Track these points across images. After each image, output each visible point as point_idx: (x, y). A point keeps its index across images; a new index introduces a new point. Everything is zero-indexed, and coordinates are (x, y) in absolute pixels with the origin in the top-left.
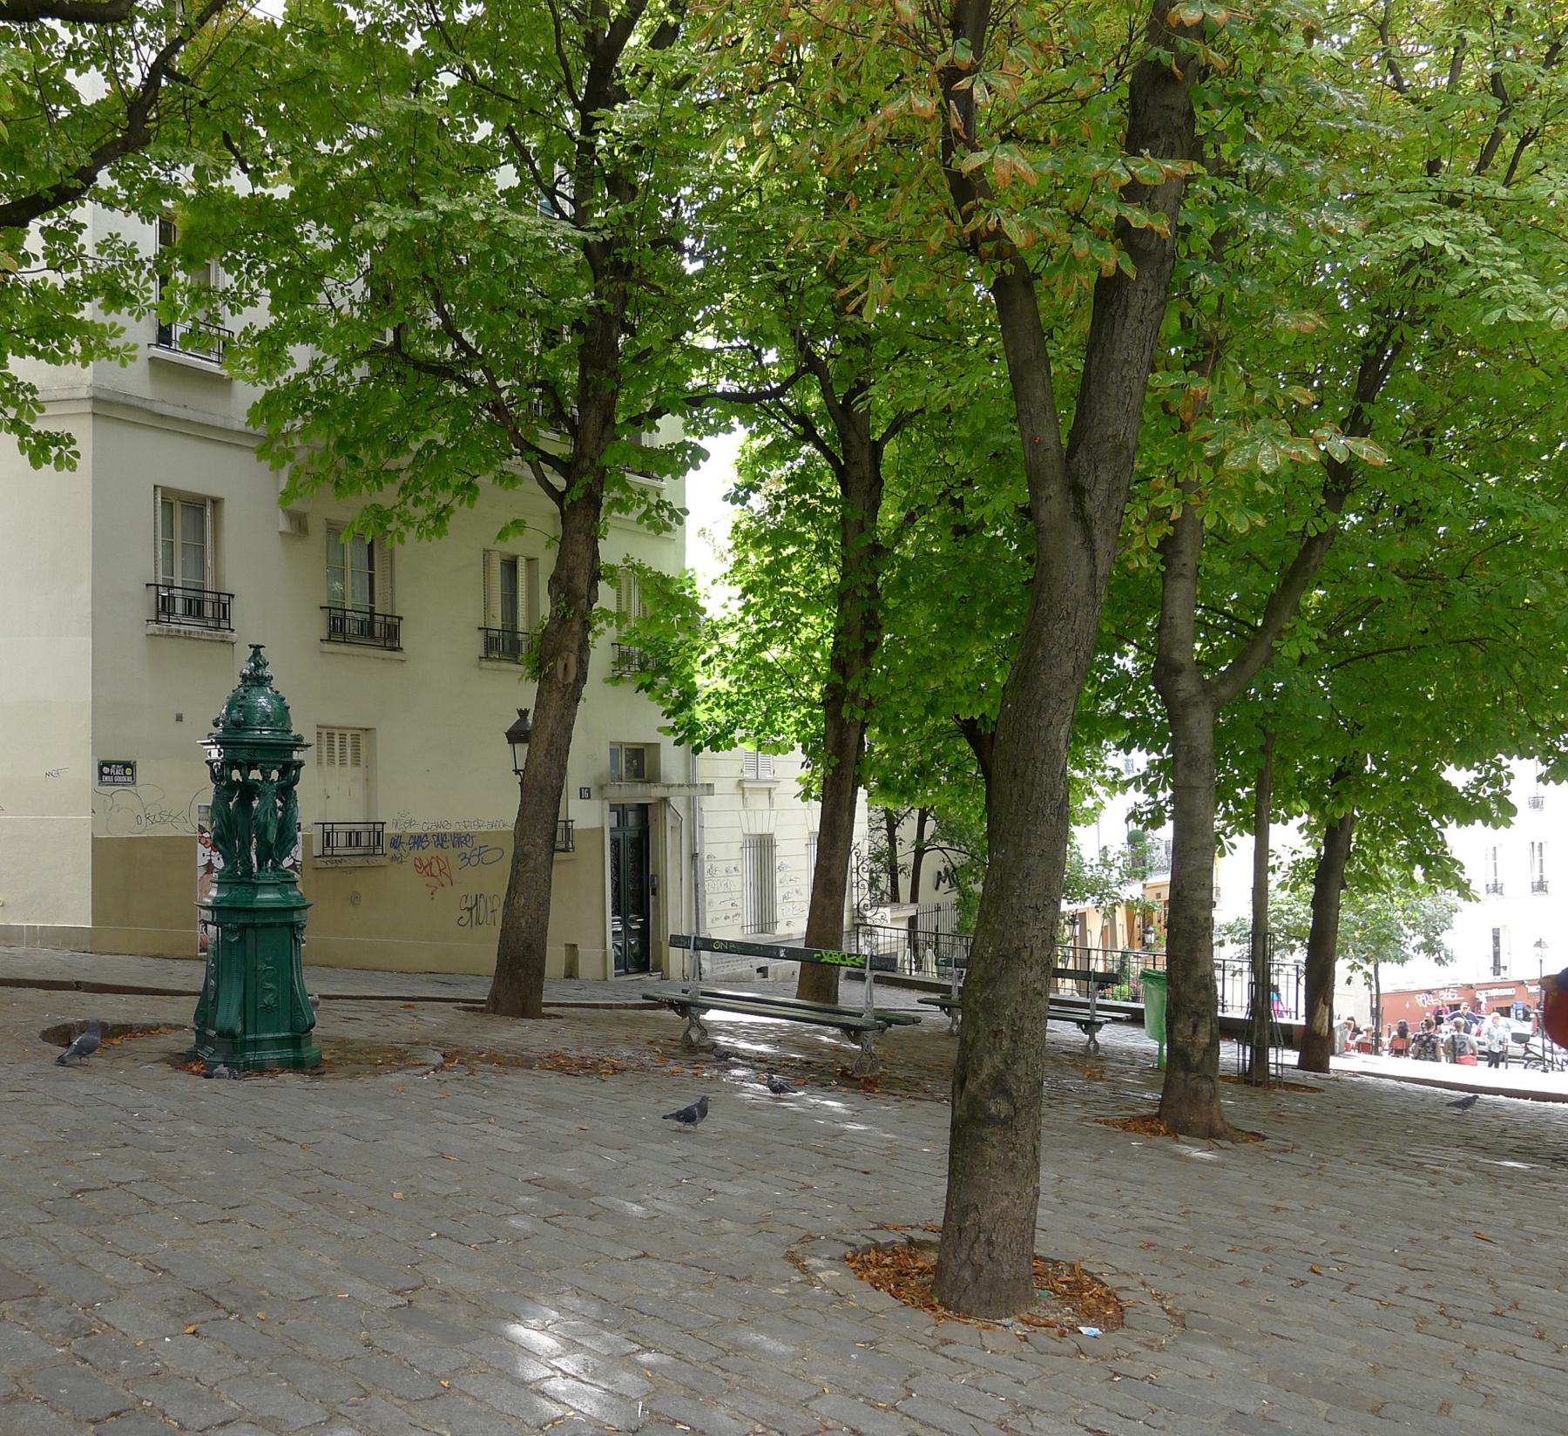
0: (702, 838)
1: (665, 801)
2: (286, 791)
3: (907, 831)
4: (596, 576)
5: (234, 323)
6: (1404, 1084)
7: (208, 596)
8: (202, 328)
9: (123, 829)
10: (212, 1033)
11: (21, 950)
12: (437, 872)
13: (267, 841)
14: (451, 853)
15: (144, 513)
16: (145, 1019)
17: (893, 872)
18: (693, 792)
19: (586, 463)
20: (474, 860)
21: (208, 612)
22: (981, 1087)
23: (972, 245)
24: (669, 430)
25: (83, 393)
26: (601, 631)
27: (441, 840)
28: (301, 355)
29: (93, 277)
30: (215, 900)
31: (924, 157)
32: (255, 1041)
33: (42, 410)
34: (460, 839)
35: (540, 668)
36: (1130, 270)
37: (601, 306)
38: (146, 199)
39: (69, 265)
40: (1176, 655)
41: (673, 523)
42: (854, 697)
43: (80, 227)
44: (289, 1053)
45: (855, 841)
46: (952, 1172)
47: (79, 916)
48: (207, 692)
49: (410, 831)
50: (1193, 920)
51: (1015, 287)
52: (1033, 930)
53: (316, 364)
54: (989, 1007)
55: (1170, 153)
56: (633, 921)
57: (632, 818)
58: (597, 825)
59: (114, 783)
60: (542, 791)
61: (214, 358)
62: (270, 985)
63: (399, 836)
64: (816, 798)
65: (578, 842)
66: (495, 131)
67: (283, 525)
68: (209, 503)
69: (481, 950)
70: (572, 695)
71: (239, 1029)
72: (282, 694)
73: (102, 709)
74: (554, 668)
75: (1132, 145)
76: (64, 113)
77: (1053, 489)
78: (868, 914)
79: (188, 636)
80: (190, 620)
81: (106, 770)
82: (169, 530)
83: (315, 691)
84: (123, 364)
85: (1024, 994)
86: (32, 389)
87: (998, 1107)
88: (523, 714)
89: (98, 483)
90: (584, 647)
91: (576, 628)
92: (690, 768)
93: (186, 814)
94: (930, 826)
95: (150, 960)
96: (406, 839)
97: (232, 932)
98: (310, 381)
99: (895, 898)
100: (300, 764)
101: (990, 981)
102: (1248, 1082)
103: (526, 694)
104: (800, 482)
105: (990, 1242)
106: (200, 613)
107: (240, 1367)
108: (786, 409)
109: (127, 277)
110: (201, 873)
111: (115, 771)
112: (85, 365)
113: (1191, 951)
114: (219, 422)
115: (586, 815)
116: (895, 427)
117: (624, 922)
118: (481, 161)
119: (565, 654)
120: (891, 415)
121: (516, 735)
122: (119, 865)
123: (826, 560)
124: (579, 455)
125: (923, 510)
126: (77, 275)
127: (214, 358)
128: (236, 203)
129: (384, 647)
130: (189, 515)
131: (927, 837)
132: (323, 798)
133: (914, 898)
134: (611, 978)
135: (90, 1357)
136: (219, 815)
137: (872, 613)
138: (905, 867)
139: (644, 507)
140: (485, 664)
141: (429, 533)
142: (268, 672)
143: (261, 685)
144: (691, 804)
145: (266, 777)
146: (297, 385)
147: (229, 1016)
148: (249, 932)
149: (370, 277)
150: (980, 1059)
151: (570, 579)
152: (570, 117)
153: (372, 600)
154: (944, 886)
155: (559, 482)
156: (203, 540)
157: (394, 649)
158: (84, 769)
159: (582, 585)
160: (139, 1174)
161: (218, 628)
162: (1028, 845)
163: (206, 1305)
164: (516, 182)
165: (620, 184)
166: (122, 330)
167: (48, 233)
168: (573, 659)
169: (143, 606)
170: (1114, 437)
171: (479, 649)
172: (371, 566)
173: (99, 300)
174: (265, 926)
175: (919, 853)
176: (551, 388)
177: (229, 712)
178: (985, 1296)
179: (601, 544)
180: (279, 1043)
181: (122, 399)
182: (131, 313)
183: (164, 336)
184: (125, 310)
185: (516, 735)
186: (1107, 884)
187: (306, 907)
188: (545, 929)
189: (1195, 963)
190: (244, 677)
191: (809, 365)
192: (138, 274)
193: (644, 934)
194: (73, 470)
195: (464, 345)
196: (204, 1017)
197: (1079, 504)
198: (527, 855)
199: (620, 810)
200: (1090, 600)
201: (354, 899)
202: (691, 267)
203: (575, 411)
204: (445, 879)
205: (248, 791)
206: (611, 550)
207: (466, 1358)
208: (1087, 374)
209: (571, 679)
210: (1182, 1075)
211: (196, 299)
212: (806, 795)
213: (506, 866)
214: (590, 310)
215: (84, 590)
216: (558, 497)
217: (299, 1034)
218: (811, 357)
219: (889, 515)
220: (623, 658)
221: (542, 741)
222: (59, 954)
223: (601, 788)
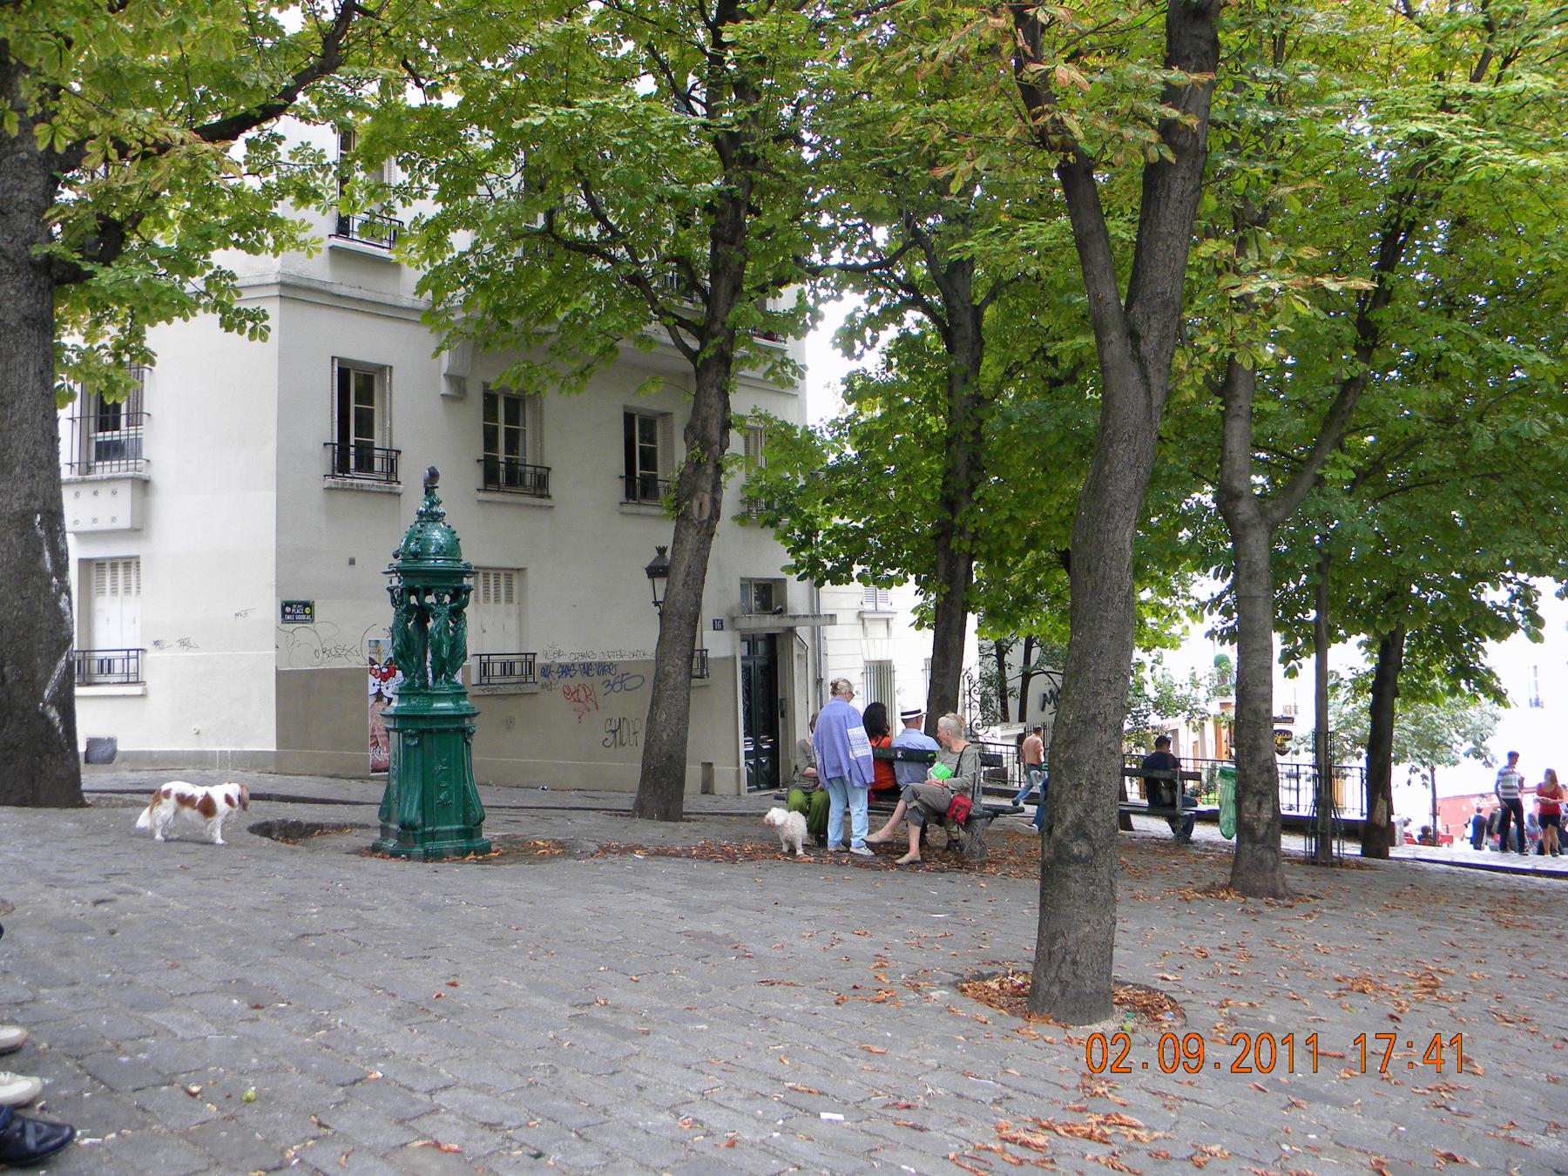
1: (791, 631)
2: (457, 613)
3: (1015, 657)
4: (726, 426)
5: (405, 214)
6: (1455, 869)
8: (378, 220)
9: (304, 662)
12: (583, 698)
14: (596, 681)
16: (333, 820)
17: (1003, 696)
18: (818, 621)
19: (717, 326)
20: (617, 687)
22: (1066, 833)
23: (1041, 140)
24: (785, 300)
25: (272, 280)
26: (733, 473)
27: (587, 669)
28: (461, 240)
29: (288, 179)
30: (397, 709)
31: (1004, 70)
32: (432, 833)
33: (239, 295)
34: (604, 668)
35: (677, 507)
36: (1170, 156)
37: (730, 191)
38: (335, 111)
39: (266, 169)
40: (1236, 484)
41: (796, 378)
42: (962, 531)
43: (281, 139)
44: (462, 843)
45: (965, 665)
46: (1042, 906)
48: (376, 539)
49: (558, 661)
50: (1256, 712)
51: (1076, 174)
52: (1106, 699)
53: (476, 245)
54: (1070, 764)
55: (1199, 70)
56: (763, 741)
57: (761, 646)
58: (728, 653)
59: (295, 621)
60: (680, 621)
61: (386, 244)
63: (549, 666)
64: (929, 627)
65: (712, 669)
66: (637, 48)
67: (444, 388)
69: (627, 768)
70: (707, 531)
72: (454, 528)
73: (287, 557)
74: (688, 507)
75: (1168, 65)
76: (268, 43)
77: (1114, 335)
78: (980, 732)
79: (360, 490)
80: (363, 475)
81: (288, 609)
83: (479, 531)
84: (310, 255)
85: (1100, 753)
86: (232, 276)
87: (1079, 848)
88: (662, 551)
89: (284, 356)
90: (717, 487)
91: (710, 470)
92: (815, 601)
94: (1036, 652)
95: (327, 780)
96: (554, 668)
97: (412, 736)
98: (471, 258)
99: (1005, 719)
100: (468, 591)
101: (1070, 743)
102: (1314, 864)
103: (665, 533)
104: (907, 343)
105: (1074, 962)
107: (452, 1053)
108: (898, 280)
109: (316, 178)
110: (371, 700)
111: (295, 611)
112: (276, 255)
113: (1255, 739)
114: (389, 300)
115: (719, 645)
116: (992, 296)
117: (756, 743)
118: (623, 74)
120: (990, 283)
121: (655, 572)
122: (299, 694)
123: (934, 411)
124: (712, 316)
125: (1020, 366)
126: (272, 178)
127: (386, 244)
128: (412, 112)
129: (534, 495)
130: (357, 388)
131: (1033, 662)
132: (487, 630)
133: (1022, 718)
134: (744, 793)
135: (332, 1044)
137: (977, 457)
138: (1014, 689)
139: (769, 364)
142: (440, 509)
143: (435, 521)
144: (816, 635)
145: (440, 601)
146: (460, 262)
147: (413, 814)
148: (426, 737)
149: (527, 170)
150: (1065, 809)
151: (704, 428)
152: (701, 35)
154: (1050, 708)
155: (694, 344)
157: (542, 496)
158: (271, 611)
159: (714, 432)
160: (353, 924)
162: (1101, 628)
163: (414, 1012)
164: (654, 89)
165: (743, 89)
166: (310, 225)
167: (250, 144)
168: (707, 499)
169: (322, 461)
170: (1163, 293)
173: (290, 199)
174: (440, 731)
175: (1026, 677)
176: (684, 262)
177: (407, 544)
178: (1071, 1007)
179: (732, 397)
181: (305, 283)
182: (318, 209)
183: (343, 228)
184: (313, 206)
185: (655, 572)
186: (1196, 701)
187: (475, 715)
188: (684, 742)
189: (1258, 749)
190: (420, 514)
191: (914, 240)
192: (326, 175)
193: (774, 753)
194: (265, 340)
195: (609, 227)
196: (386, 811)
197: (1136, 347)
198: (668, 675)
199: (750, 640)
200: (1148, 427)
201: (509, 723)
202: (808, 155)
203: (708, 284)
204: (591, 705)
206: (741, 403)
207: (637, 1049)
208: (1139, 244)
209: (705, 517)
210: (1249, 846)
211: (372, 194)
212: (919, 625)
213: (647, 694)
214: (720, 194)
215: (270, 450)
216: (692, 355)
217: (471, 830)
218: (917, 234)
219: (990, 369)
220: (750, 501)
221: (676, 578)
223: (733, 619)
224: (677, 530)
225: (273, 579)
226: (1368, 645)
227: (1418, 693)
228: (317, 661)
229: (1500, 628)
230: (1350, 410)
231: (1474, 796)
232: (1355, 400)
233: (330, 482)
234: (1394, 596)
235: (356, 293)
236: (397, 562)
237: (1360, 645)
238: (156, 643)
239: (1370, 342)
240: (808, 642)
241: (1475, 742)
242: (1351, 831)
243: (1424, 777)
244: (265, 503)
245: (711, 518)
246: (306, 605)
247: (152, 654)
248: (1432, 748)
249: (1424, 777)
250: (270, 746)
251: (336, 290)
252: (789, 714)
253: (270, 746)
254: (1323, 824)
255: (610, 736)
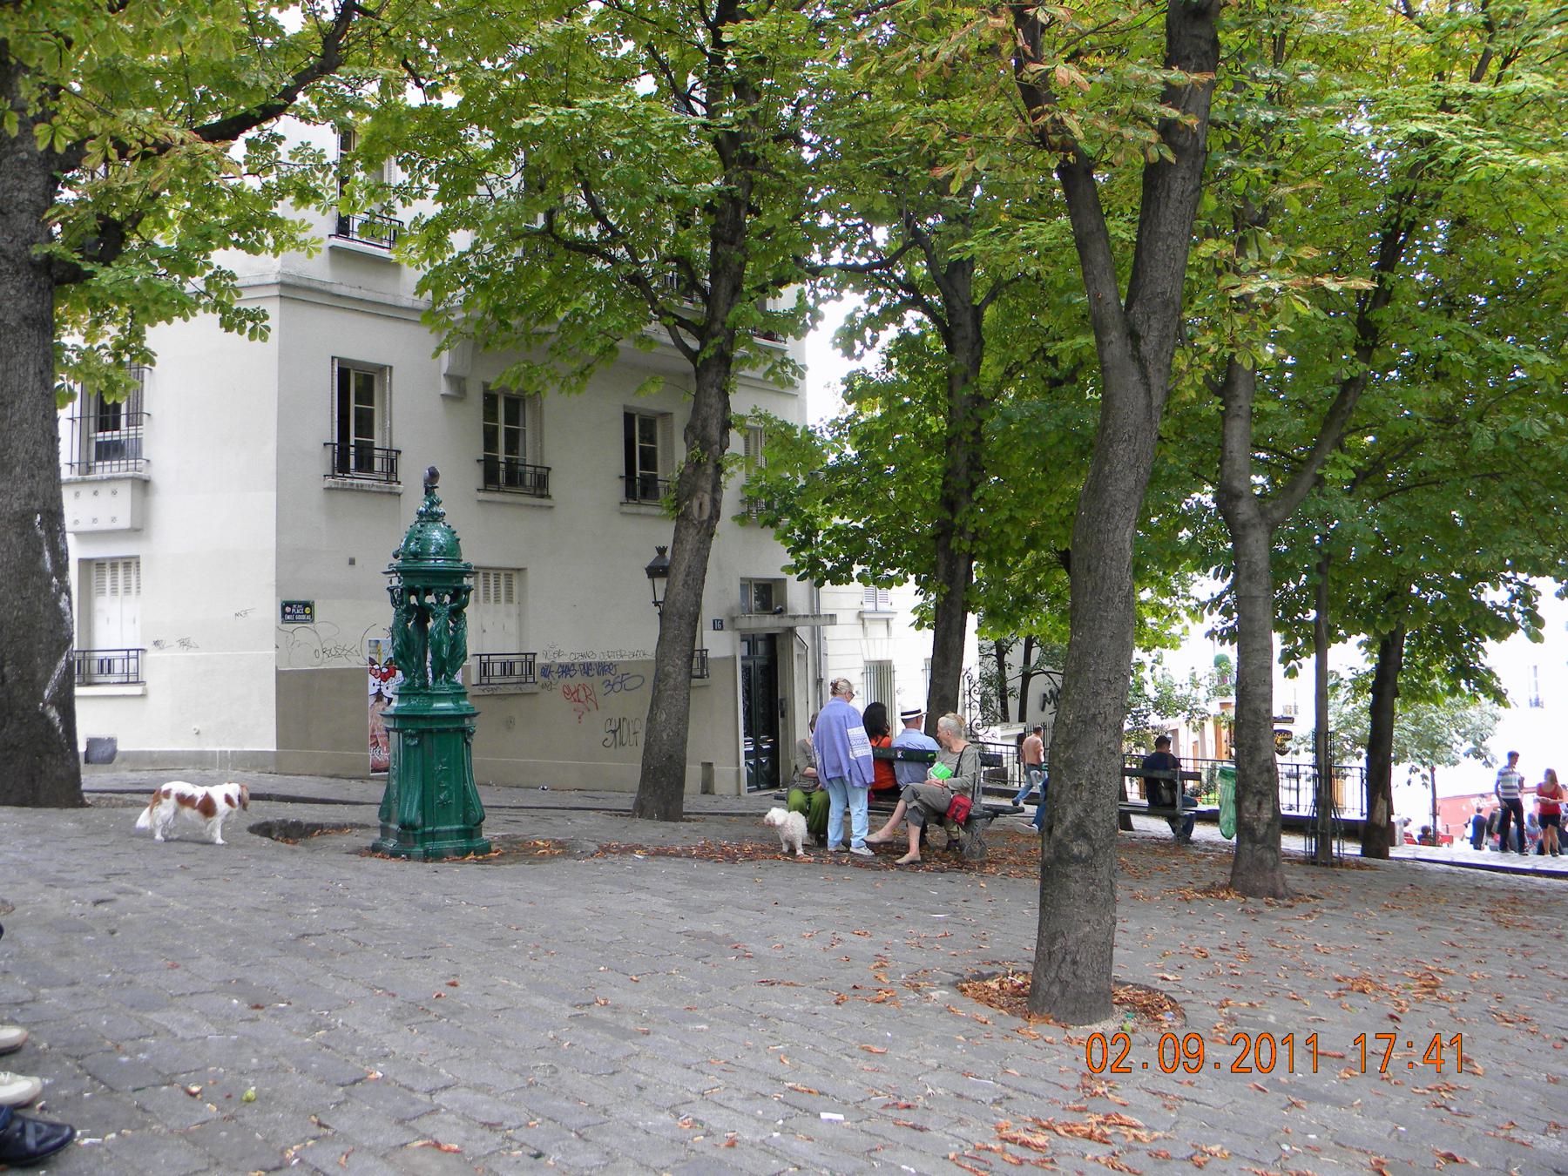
1: (791, 631)
2: (457, 613)
3: (1015, 657)
4: (726, 426)
5: (405, 214)
6: (1455, 869)
8: (378, 220)
9: (304, 662)
12: (583, 698)
14: (596, 681)
16: (333, 820)
17: (1003, 696)
18: (818, 621)
19: (717, 326)
20: (617, 687)
22: (1066, 833)
23: (1041, 140)
24: (785, 300)
25: (272, 280)
26: (733, 473)
27: (587, 669)
28: (461, 240)
29: (288, 179)
30: (397, 709)
31: (1004, 70)
32: (432, 833)
33: (239, 295)
34: (604, 668)
35: (677, 507)
36: (1170, 156)
37: (730, 191)
38: (335, 111)
39: (266, 169)
40: (1236, 484)
41: (796, 378)
42: (962, 531)
43: (281, 139)
44: (462, 843)
45: (965, 665)
46: (1042, 906)
48: (376, 539)
49: (558, 661)
50: (1256, 712)
51: (1076, 174)
52: (1106, 699)
53: (476, 245)
54: (1070, 764)
56: (763, 741)
57: (761, 646)
58: (728, 653)
59: (295, 621)
60: (680, 621)
61: (386, 244)
63: (549, 666)
64: (929, 627)
65: (712, 669)
66: (637, 48)
67: (444, 388)
69: (627, 768)
70: (707, 531)
72: (454, 528)
73: (287, 557)
74: (688, 507)
76: (268, 43)
77: (1114, 335)
78: (980, 732)
79: (360, 490)
80: (363, 475)
81: (288, 609)
83: (479, 531)
84: (310, 255)
85: (1100, 753)
86: (232, 276)
87: (1079, 848)
88: (662, 551)
89: (284, 356)
90: (717, 487)
91: (710, 470)
92: (815, 601)
94: (1036, 652)
95: (327, 780)
96: (554, 668)
97: (412, 736)
99: (1005, 719)
100: (468, 591)
101: (1070, 743)
102: (1314, 864)
103: (665, 533)
104: (907, 343)
105: (1074, 962)
107: (452, 1053)
108: (898, 280)
109: (316, 178)
110: (371, 700)
111: (295, 611)
112: (276, 255)
113: (1255, 739)
114: (389, 300)
115: (719, 645)
116: (992, 296)
117: (756, 743)
118: (623, 74)
120: (990, 283)
121: (655, 572)
122: (299, 694)
123: (934, 411)
124: (712, 316)
125: (1020, 366)
126: (272, 178)
127: (386, 244)
128: (412, 112)
129: (534, 495)
130: (357, 388)
131: (1033, 662)
132: (487, 630)
133: (1022, 718)
134: (744, 793)
135: (332, 1044)
137: (977, 457)
138: (1014, 689)
139: (769, 364)
142: (440, 509)
143: (435, 521)
144: (816, 635)
145: (440, 601)
147: (413, 814)
148: (426, 737)
149: (527, 170)
150: (1065, 809)
151: (704, 428)
152: (701, 35)
154: (1050, 708)
155: (694, 344)
157: (542, 496)
158: (271, 611)
159: (714, 432)
160: (353, 924)
162: (1101, 628)
163: (414, 1012)
164: (654, 89)
165: (743, 89)
166: (310, 225)
167: (250, 144)
168: (707, 499)
169: (322, 461)
170: (1163, 293)
173: (290, 199)
174: (440, 731)
175: (1026, 677)
176: (684, 262)
177: (407, 544)
178: (1071, 1007)
179: (732, 397)
181: (305, 283)
182: (318, 209)
183: (343, 228)
184: (313, 206)
185: (655, 572)
186: (1196, 701)
187: (475, 715)
188: (684, 742)
189: (1258, 749)
190: (420, 514)
191: (914, 240)
192: (326, 175)
193: (774, 753)
194: (265, 340)
195: (609, 227)
196: (386, 811)
197: (1136, 347)
198: (668, 675)
199: (750, 640)
200: (1148, 427)
201: (509, 723)
202: (808, 155)
203: (708, 284)
204: (591, 705)
206: (741, 403)
207: (637, 1049)
208: (1139, 244)
209: (705, 517)
210: (1249, 846)
211: (372, 194)
212: (919, 625)
213: (647, 694)
214: (720, 194)
215: (270, 450)
216: (692, 355)
217: (471, 830)
218: (917, 234)
219: (990, 369)
220: (750, 501)
221: (676, 578)
223: (733, 619)
224: (677, 530)
225: (273, 579)
226: (1368, 645)
227: (1418, 693)
228: (317, 661)
229: (1500, 628)
230: (1350, 410)
231: (1474, 796)
232: (1355, 400)
233: (330, 482)
234: (1394, 596)
235: (356, 293)
236: (397, 562)
237: (1360, 645)
238: (156, 643)
239: (1370, 342)
240: (808, 642)
241: (1475, 742)
242: (1351, 831)
243: (1424, 777)
244: (265, 503)
245: (711, 518)
246: (306, 605)
247: (152, 654)
248: (1432, 748)
249: (1424, 777)
250: (270, 746)
251: (336, 290)
252: (789, 714)
253: (270, 746)
254: (1323, 824)
255: (610, 736)
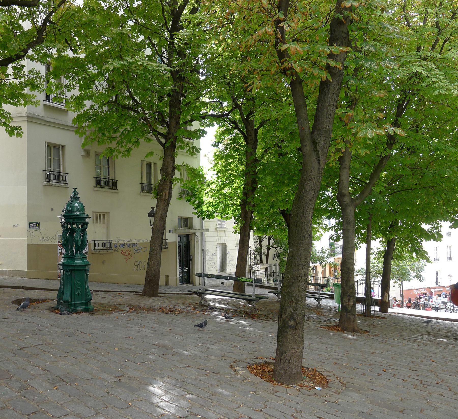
0: (205, 245)
1: (194, 234)
2: (84, 231)
4: (174, 168)
5: (68, 94)
6: (410, 316)
7: (61, 174)
8: (59, 96)
9: (36, 242)
10: (62, 301)
11: (6, 277)
12: (128, 255)
13: (78, 245)
14: (132, 249)
15: (42, 150)
16: (42, 297)
18: (202, 231)
19: (171, 135)
20: (138, 251)
21: (61, 178)
22: (287, 317)
23: (284, 72)
24: (195, 125)
25: (24, 115)
26: (176, 184)
27: (129, 245)
28: (88, 104)
29: (27, 81)
30: (63, 263)
31: (270, 46)
32: (75, 304)
33: (12, 120)
34: (134, 245)
35: (158, 195)
36: (330, 79)
37: (175, 89)
38: (43, 58)
39: (20, 77)
40: (344, 191)
41: (197, 153)
43: (23, 66)
44: (84, 307)
46: (278, 342)
47: (23, 267)
48: (61, 202)
49: (120, 242)
50: (348, 269)
51: (297, 84)
52: (302, 271)
54: (289, 294)
56: (185, 269)
57: (185, 239)
58: (174, 241)
59: (33, 229)
60: (158, 231)
61: (63, 104)
62: (79, 288)
63: (117, 244)
65: (169, 246)
66: (144, 38)
67: (83, 153)
68: (61, 147)
69: (140, 277)
70: (167, 203)
71: (70, 300)
72: (82, 202)
73: (30, 207)
74: (162, 195)
76: (19, 33)
77: (308, 143)
79: (55, 186)
80: (56, 181)
81: (31, 225)
82: (49, 155)
83: (92, 202)
84: (36, 106)
85: (299, 290)
86: (9, 113)
87: (292, 323)
88: (153, 208)
89: (29, 141)
90: (171, 189)
91: (168, 183)
92: (202, 224)
93: (54, 237)
95: (44, 280)
96: (118, 245)
97: (68, 272)
100: (88, 223)
101: (289, 286)
102: (364, 316)
103: (154, 202)
104: (234, 141)
105: (289, 363)
106: (58, 179)
107: (70, 399)
109: (37, 81)
110: (59, 255)
111: (34, 225)
112: (25, 107)
113: (348, 278)
114: (64, 123)
115: (171, 238)
117: (182, 269)
118: (140, 47)
119: (165, 191)
121: (151, 215)
122: (35, 253)
124: (169, 133)
126: (22, 80)
127: (63, 104)
128: (69, 59)
129: (112, 189)
130: (55, 150)
132: (94, 233)
134: (179, 285)
135: (26, 396)
136: (64, 238)
139: (188, 148)
140: (142, 194)
141: (125, 155)
142: (78, 196)
143: (76, 200)
144: (202, 235)
145: (78, 227)
147: (67, 296)
148: (73, 272)
149: (108, 81)
150: (286, 309)
151: (166, 169)
152: (166, 34)
153: (109, 175)
155: (163, 141)
156: (59, 158)
157: (115, 189)
158: (24, 224)
159: (170, 171)
160: (41, 342)
161: (64, 183)
162: (300, 246)
163: (60, 381)
164: (151, 53)
165: (181, 54)
166: (36, 96)
167: (14, 68)
168: (167, 192)
169: (42, 177)
170: (325, 127)
171: (140, 189)
172: (108, 165)
173: (29, 88)
174: (77, 270)
176: (161, 113)
177: (67, 208)
178: (288, 378)
179: (176, 159)
180: (81, 304)
181: (36, 117)
182: (38, 91)
183: (48, 98)
184: (37, 90)
185: (151, 215)
187: (89, 265)
188: (159, 271)
189: (349, 281)
190: (71, 197)
192: (40, 80)
193: (188, 272)
194: (21, 137)
195: (135, 101)
196: (60, 297)
197: (315, 147)
198: (154, 250)
199: (181, 236)
200: (318, 175)
201: (104, 262)
202: (202, 78)
203: (168, 120)
204: (130, 257)
205: (72, 231)
206: (179, 161)
207: (136, 396)
208: (317, 109)
209: (167, 198)
210: (345, 314)
211: (57, 87)
212: (235, 232)
213: (148, 253)
214: (172, 90)
215: (25, 172)
216: (163, 145)
217: (87, 302)
220: (182, 192)
221: (158, 216)
222: (17, 278)
223: (176, 230)
226: (383, 242)
227: (400, 257)
229: (429, 236)
230: (384, 166)
231: (415, 289)
232: (386, 162)
234: (393, 226)
237: (380, 242)
239: (392, 142)
241: (417, 273)
242: (376, 303)
243: (399, 284)
248: (404, 276)
249: (399, 284)
254: (367, 300)
